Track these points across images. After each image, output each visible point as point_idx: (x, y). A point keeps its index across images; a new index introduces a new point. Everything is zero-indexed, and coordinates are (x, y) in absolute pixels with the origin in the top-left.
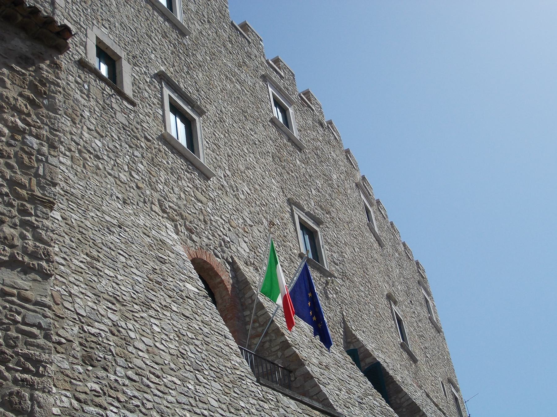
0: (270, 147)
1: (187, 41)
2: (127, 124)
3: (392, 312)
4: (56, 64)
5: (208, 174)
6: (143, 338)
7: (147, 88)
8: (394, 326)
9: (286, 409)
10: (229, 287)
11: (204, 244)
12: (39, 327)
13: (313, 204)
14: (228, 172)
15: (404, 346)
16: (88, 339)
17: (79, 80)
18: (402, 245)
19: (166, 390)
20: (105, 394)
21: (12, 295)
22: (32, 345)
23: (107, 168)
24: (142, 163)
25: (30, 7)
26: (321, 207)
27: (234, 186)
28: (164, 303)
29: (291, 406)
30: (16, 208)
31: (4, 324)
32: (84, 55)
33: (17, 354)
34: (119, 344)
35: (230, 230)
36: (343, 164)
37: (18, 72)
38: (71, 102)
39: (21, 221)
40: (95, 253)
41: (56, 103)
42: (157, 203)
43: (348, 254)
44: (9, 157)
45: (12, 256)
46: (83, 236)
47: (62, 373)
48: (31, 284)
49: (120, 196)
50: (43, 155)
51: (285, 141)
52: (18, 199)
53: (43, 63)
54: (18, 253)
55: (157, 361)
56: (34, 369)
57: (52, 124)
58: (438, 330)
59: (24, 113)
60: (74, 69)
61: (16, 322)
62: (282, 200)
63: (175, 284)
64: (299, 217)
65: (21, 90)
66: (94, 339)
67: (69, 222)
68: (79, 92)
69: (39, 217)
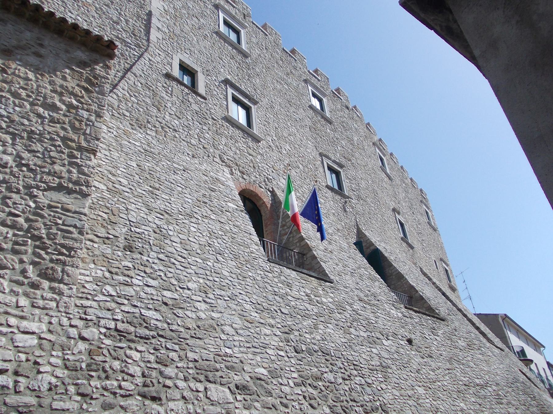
0: (308, 122)
1: (249, 60)
2: (199, 110)
3: (396, 219)
4: (107, 66)
5: (259, 139)
6: (179, 235)
7: (216, 89)
8: (397, 227)
9: (287, 277)
10: (269, 206)
11: (252, 180)
12: (75, 227)
13: (338, 155)
14: (275, 138)
15: (405, 238)
16: (132, 236)
17: (165, 85)
18: (409, 180)
19: (188, 266)
20: (135, 268)
21: (58, 207)
22: (68, 238)
23: (182, 137)
24: (208, 133)
25: (72, 24)
26: (344, 157)
27: (279, 146)
28: (205, 214)
29: (291, 275)
30: (66, 154)
31: (48, 225)
32: (170, 70)
33: (55, 244)
34: (158, 238)
35: (273, 172)
36: (363, 131)
37: (77, 71)
38: (158, 98)
39: (69, 162)
40: (157, 186)
41: (104, 90)
42: (218, 157)
43: (363, 184)
44: (64, 123)
45: (60, 184)
46: (151, 176)
47: (104, 256)
48: (73, 201)
49: (190, 153)
50: (91, 121)
51: (319, 118)
52: (68, 148)
53: (97, 65)
54: (64, 182)
55: (187, 249)
56: (68, 253)
57: (100, 102)
58: (435, 230)
59: (78, 96)
60: (162, 79)
61: (57, 224)
62: (315, 154)
63: (219, 203)
64: (327, 163)
65: (78, 82)
66: (138, 235)
67: (143, 168)
68: (164, 92)
69: (83, 159)
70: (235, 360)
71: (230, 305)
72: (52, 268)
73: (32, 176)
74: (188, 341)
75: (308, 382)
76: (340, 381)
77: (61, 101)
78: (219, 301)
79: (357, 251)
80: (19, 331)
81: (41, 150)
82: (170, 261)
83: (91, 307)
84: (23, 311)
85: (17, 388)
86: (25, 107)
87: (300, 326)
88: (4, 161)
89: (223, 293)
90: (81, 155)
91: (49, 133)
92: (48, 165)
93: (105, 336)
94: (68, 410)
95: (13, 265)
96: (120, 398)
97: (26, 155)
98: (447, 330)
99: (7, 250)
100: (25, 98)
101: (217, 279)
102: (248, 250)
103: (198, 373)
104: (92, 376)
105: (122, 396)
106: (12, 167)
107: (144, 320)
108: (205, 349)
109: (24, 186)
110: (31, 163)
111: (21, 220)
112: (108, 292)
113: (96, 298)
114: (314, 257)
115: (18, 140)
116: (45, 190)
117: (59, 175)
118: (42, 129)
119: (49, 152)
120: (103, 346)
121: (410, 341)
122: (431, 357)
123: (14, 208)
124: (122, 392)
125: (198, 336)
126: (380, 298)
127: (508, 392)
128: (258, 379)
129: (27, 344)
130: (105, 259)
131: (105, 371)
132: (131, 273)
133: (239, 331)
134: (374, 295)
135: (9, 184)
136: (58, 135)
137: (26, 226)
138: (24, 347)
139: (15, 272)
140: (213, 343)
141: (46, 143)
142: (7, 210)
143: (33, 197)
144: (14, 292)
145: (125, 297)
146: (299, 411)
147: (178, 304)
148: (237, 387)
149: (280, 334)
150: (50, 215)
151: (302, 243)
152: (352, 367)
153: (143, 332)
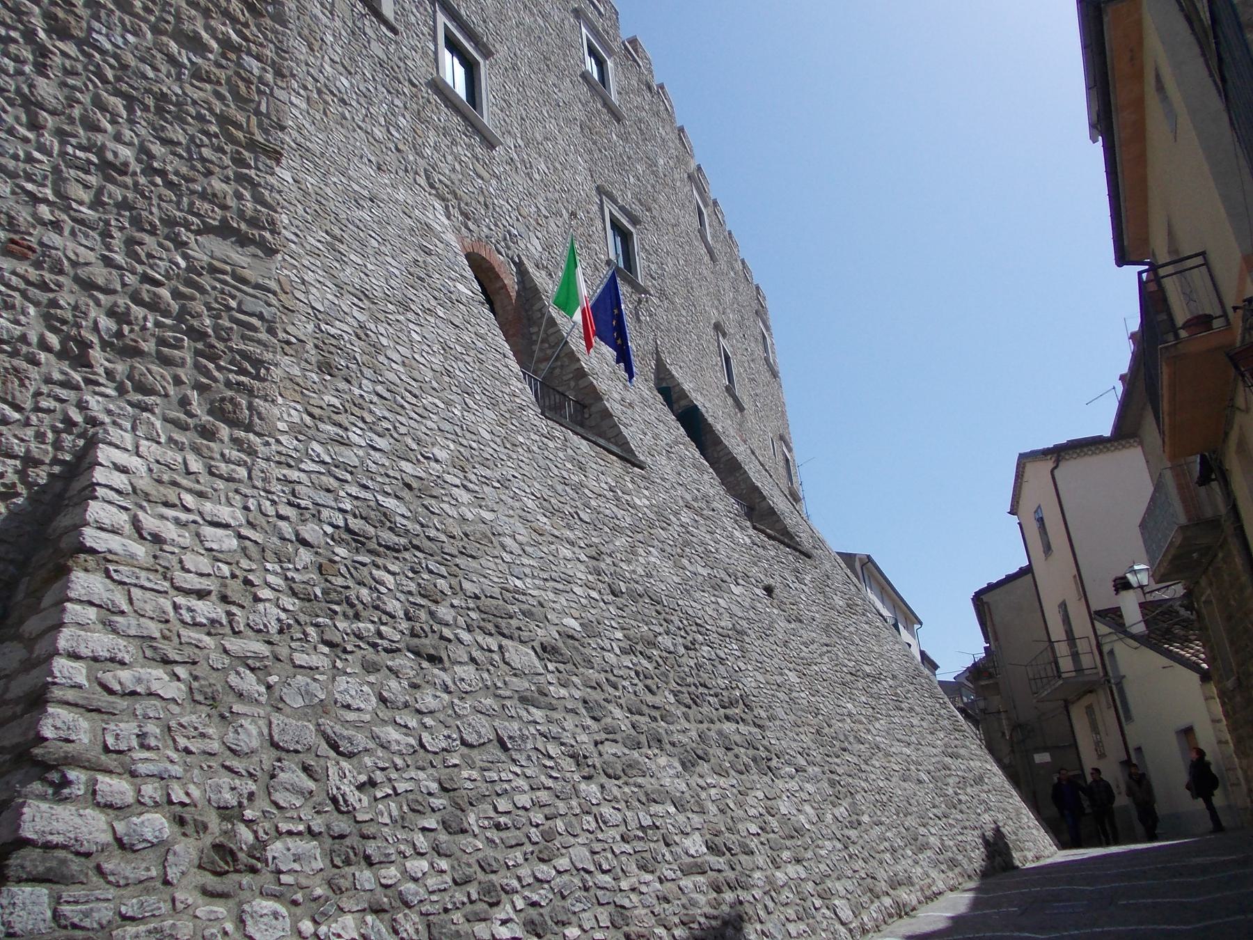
0: (578, 112)
10: (513, 294)
12: (261, 317)
14: (519, 141)
19: (426, 414)
21: (224, 272)
26: (640, 201)
33: (231, 349)
39: (235, 173)
42: (422, 174)
43: (670, 267)
44: (219, 83)
45: (224, 221)
48: (249, 260)
49: (373, 159)
50: (267, 85)
58: (775, 375)
62: (589, 187)
66: (334, 342)
70: (531, 600)
71: (503, 497)
72: (232, 400)
73: (174, 198)
74: (457, 561)
75: (638, 648)
76: (682, 650)
77: (208, 28)
78: (486, 488)
79: (666, 408)
80: (204, 519)
81: (184, 142)
82: (395, 402)
83: (299, 483)
84: (198, 482)
85: (235, 625)
86: (144, 35)
87: (611, 547)
88: (122, 159)
89: (488, 473)
90: (256, 160)
91: (194, 103)
92: (200, 178)
93: (333, 539)
94: (317, 668)
95: (164, 388)
96: (383, 653)
97: (157, 149)
98: (816, 575)
99: (149, 354)
100: (142, 13)
101: (474, 445)
102: (507, 390)
103: (483, 620)
104: (336, 613)
105: (387, 650)
106: (135, 174)
107: (385, 515)
108: (484, 576)
109: (161, 219)
110: (169, 168)
111: (165, 293)
112: (318, 456)
113: (303, 466)
114: (607, 414)
115: (139, 113)
116: (198, 232)
117: (222, 201)
118: (180, 92)
119: (199, 146)
120: (337, 558)
121: (769, 590)
122: (801, 621)
123: (151, 267)
124: (385, 643)
125: (469, 552)
126: (715, 505)
127: (909, 691)
128: (569, 636)
129: (225, 547)
130: (297, 388)
131: (352, 605)
132: (341, 418)
133: (527, 548)
134: (706, 499)
135: (134, 213)
136: (211, 110)
137: (175, 306)
138: (221, 552)
139: (169, 403)
140: (494, 567)
141: (189, 124)
142: (139, 268)
143: (181, 245)
144: (176, 443)
145: (345, 467)
146: (633, 697)
147: (427, 488)
148: (544, 649)
149: (586, 559)
150: (214, 288)
151: (582, 383)
152: (694, 628)
153: (388, 537)
